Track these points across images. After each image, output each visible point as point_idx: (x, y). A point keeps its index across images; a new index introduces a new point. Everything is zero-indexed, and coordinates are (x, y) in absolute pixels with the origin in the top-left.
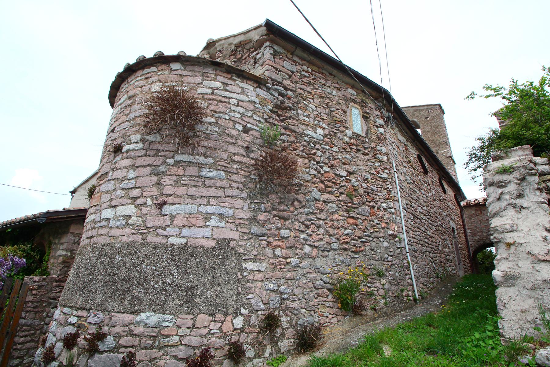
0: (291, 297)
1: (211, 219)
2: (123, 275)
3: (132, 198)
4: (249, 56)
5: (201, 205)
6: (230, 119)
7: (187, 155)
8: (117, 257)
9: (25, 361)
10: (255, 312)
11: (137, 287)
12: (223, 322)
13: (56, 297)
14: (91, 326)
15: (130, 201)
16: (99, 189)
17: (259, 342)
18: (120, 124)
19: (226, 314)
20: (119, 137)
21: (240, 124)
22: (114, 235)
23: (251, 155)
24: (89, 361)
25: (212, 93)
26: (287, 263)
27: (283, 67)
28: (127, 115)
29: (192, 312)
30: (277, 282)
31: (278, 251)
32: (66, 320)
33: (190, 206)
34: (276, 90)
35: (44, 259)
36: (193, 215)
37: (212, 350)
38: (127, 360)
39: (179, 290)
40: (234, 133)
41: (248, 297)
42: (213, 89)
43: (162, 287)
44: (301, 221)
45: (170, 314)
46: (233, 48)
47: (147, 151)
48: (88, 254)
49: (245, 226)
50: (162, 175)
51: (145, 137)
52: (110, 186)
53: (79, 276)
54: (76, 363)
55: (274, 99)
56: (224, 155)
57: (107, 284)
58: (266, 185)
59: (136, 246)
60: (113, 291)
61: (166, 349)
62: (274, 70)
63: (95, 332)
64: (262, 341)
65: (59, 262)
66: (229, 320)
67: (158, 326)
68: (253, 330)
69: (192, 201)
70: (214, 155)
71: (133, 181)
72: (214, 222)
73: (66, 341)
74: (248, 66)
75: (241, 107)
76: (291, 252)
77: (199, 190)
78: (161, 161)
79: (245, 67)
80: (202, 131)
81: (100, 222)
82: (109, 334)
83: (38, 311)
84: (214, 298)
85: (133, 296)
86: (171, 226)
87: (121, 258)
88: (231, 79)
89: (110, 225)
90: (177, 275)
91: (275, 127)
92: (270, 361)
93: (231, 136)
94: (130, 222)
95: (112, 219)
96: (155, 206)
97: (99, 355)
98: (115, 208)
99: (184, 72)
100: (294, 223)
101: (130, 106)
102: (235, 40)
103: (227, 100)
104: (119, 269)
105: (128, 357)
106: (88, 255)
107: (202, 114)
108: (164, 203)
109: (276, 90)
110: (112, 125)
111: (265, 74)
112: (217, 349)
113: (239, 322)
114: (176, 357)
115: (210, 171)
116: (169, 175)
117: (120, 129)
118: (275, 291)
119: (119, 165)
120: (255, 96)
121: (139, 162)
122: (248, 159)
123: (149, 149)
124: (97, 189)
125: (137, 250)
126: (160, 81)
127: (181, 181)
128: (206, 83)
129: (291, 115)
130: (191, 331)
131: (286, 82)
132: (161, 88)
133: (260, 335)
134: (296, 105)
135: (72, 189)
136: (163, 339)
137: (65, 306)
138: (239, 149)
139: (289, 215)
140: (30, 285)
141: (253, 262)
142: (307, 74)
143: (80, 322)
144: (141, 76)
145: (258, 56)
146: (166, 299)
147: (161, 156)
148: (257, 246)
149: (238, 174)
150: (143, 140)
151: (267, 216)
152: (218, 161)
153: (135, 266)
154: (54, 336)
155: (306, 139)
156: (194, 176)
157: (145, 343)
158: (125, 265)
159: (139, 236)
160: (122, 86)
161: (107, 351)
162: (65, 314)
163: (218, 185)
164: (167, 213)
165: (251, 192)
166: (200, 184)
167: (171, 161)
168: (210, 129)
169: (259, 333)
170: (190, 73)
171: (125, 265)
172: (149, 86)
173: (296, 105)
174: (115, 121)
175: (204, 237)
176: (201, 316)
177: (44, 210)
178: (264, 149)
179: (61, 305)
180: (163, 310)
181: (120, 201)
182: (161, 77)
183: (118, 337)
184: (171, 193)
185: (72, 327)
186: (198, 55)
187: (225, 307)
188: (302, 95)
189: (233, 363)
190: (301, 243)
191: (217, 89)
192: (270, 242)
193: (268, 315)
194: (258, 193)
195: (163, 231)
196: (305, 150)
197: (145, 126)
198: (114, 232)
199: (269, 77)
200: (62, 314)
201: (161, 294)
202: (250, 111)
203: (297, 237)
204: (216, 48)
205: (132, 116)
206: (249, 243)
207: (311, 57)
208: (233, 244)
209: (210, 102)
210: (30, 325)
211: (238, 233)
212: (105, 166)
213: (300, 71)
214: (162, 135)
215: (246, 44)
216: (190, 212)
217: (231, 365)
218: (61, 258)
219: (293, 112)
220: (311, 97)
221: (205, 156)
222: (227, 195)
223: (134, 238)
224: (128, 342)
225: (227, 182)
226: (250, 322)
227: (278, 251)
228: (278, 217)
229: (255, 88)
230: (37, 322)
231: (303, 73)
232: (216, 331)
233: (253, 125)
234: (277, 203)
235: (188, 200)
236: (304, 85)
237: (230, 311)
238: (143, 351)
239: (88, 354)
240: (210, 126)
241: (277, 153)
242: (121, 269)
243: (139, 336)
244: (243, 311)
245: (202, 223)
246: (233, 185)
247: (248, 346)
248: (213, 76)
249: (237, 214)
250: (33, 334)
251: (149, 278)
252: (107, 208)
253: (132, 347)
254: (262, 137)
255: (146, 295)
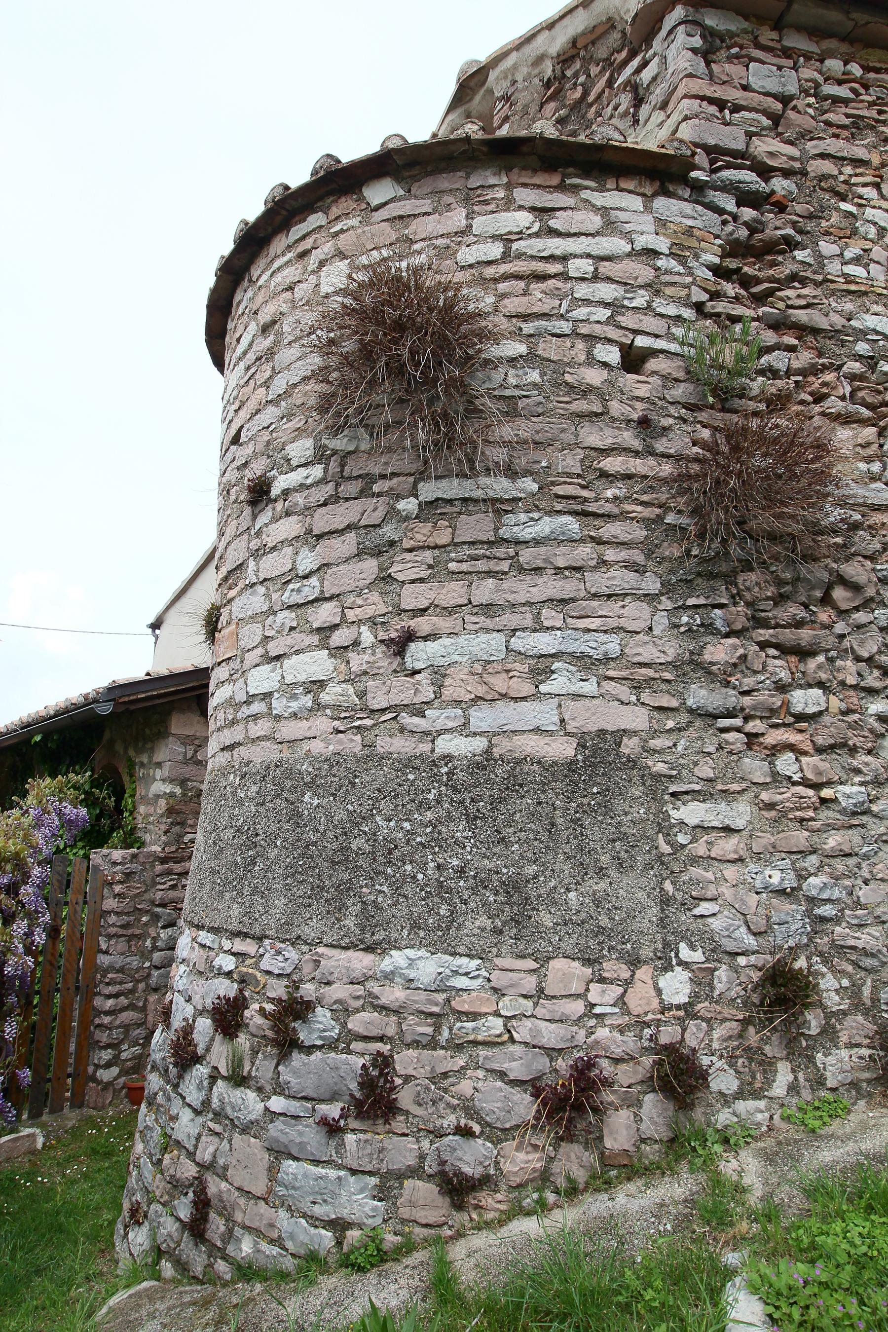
0: (847, 912)
1: (553, 672)
2: (329, 845)
3: (319, 630)
4: (610, 83)
5: (515, 630)
6: (575, 334)
7: (456, 481)
8: (306, 798)
9: (124, 1056)
10: (726, 959)
11: (371, 878)
12: (628, 983)
13: (166, 901)
14: (271, 981)
15: (315, 639)
16: (230, 615)
17: (748, 1049)
18: (253, 415)
19: (635, 962)
20: (255, 455)
21: (610, 341)
22: (287, 739)
23: (660, 446)
24: (280, 1068)
25: (506, 256)
26: (823, 801)
27: (745, 88)
28: (267, 384)
29: (531, 951)
30: (793, 863)
31: (786, 764)
32: (209, 962)
33: (483, 637)
34: (727, 188)
35: (125, 807)
36: (495, 665)
37: (604, 1063)
38: (375, 1073)
39: (486, 887)
40: (594, 377)
41: (697, 911)
42: (506, 240)
43: (438, 880)
44: (866, 655)
45: (470, 956)
46: (549, 73)
47: (338, 485)
48: (232, 792)
49: (664, 687)
50: (391, 552)
51: (327, 442)
52: (256, 601)
53: (221, 850)
54: (249, 1072)
55: (724, 223)
56: (569, 461)
57: (292, 871)
58: (724, 541)
59: (352, 765)
60: (312, 889)
61: (473, 1051)
62: (713, 109)
63: (285, 997)
64: (760, 1048)
65: (159, 812)
66: (644, 978)
67: (441, 987)
68: (728, 1012)
69: (489, 623)
70: (537, 466)
71: (314, 581)
72: (558, 684)
73: (217, 1016)
74: (613, 121)
75: (609, 279)
76: (835, 764)
77: (506, 585)
78: (380, 509)
79: (605, 129)
80: (489, 392)
81: (247, 703)
82: (319, 1001)
83: (134, 936)
84: (592, 912)
85: (364, 903)
86: (436, 703)
87: (316, 802)
88: (561, 188)
89: (274, 712)
90: (475, 845)
91: (738, 328)
92: (793, 1111)
93: (587, 391)
94: (325, 697)
95: (276, 695)
96: (383, 647)
97: (303, 1056)
98: (279, 664)
99: (407, 207)
100: (839, 663)
101: (270, 353)
102: (553, 39)
103: (554, 268)
104: (318, 830)
105: (374, 1066)
106: (234, 794)
107: (484, 335)
108: (409, 637)
109: (727, 188)
110: (231, 422)
111: (679, 135)
112: (617, 1061)
113: (678, 985)
114: (502, 1075)
115: (532, 519)
116: (410, 550)
117: (256, 429)
118: (788, 895)
119: (269, 539)
120: (652, 228)
121: (322, 521)
122: (651, 461)
123: (342, 477)
124: (225, 611)
125: (356, 777)
126: (341, 255)
127: (447, 562)
128: (480, 224)
129: (795, 268)
130: (536, 1004)
131: (763, 147)
132: (350, 277)
133: (751, 1030)
134: (809, 226)
135: (151, 619)
136: (459, 1024)
137: (200, 927)
138: (617, 433)
139: (815, 636)
140: (106, 872)
141: (704, 801)
142: (843, 91)
143: (245, 970)
144: (283, 254)
145: (646, 75)
146: (452, 912)
147: (379, 495)
148: (712, 749)
149: (623, 516)
150: (322, 455)
151: (735, 648)
152: (553, 484)
153: (357, 820)
154: (187, 1001)
155: (862, 348)
156: (482, 542)
157: (414, 1032)
158: (330, 818)
159: (355, 738)
160: (237, 298)
161: (320, 1048)
162: (203, 946)
163: (561, 563)
164: (419, 665)
165: (672, 572)
166: (505, 566)
167: (408, 505)
168: (512, 381)
169: (745, 1023)
170: (426, 205)
171: (330, 818)
172: (313, 279)
173: (809, 226)
174: (236, 411)
175: (537, 730)
176: (558, 965)
177: (104, 683)
178: (703, 416)
179: (191, 924)
180: (449, 945)
181: (289, 641)
182: (344, 241)
183: (342, 1011)
184: (425, 603)
185: (227, 982)
186: (434, 135)
187: (628, 941)
188: (832, 182)
189: (671, 1106)
190: (871, 731)
191: (520, 235)
192: (757, 735)
193: (773, 967)
194: (699, 574)
195: (416, 720)
196: (861, 394)
197: (322, 410)
198: (290, 730)
199: (696, 145)
200: (196, 946)
201: (436, 899)
202: (641, 287)
203: (854, 711)
204: (491, 92)
205: (280, 385)
206: (682, 742)
207: (855, 15)
208: (630, 746)
209: (502, 287)
210: (121, 970)
211: (643, 712)
212: (232, 546)
213: (817, 86)
214: (373, 426)
215: (593, 43)
216: (485, 658)
217: (666, 1109)
218: (162, 803)
219: (800, 255)
220: (869, 179)
221: (512, 473)
222: (593, 591)
223: (340, 742)
224: (370, 1027)
225: (588, 550)
226: (712, 988)
227: (786, 764)
228: (777, 646)
229: (648, 199)
230: (134, 962)
231: (830, 89)
232: (608, 1010)
233: (657, 336)
234: (768, 598)
235: (475, 619)
236: (836, 136)
237: (646, 952)
238: (412, 1053)
239: (275, 1051)
240: (512, 372)
241: (754, 423)
242: (321, 830)
243: (396, 1012)
244: (685, 952)
245: (527, 688)
246: (611, 554)
247: (714, 1059)
248: (501, 194)
249: (635, 651)
250: (132, 991)
251: (397, 853)
252: (257, 665)
253: (381, 1039)
254: (691, 376)
255: (397, 901)
